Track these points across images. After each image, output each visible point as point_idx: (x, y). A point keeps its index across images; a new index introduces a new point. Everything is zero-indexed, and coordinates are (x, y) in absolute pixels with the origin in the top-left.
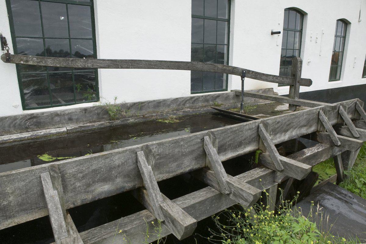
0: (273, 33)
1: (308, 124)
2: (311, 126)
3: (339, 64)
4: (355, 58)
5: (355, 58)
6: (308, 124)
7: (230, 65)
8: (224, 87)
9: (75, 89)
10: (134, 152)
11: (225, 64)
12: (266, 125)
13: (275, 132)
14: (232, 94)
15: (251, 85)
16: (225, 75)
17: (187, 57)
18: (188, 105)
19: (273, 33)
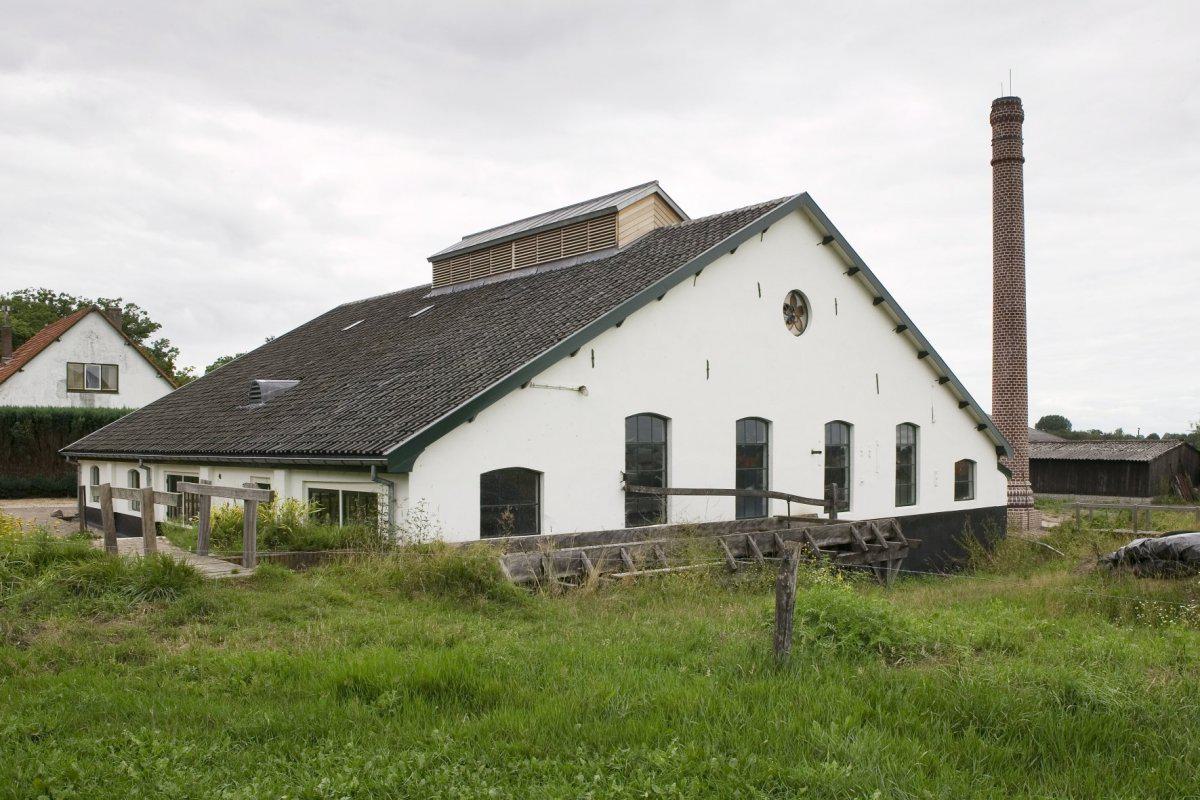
0: (813, 452)
1: (841, 535)
2: (845, 538)
3: (970, 479)
4: (936, 473)
5: (936, 473)
6: (841, 535)
7: (669, 486)
8: (764, 514)
9: (238, 575)
10: (747, 536)
11: (663, 486)
12: (809, 530)
13: (816, 537)
14: (775, 519)
15: (797, 509)
16: (764, 499)
17: (732, 485)
18: (738, 528)
19: (813, 452)
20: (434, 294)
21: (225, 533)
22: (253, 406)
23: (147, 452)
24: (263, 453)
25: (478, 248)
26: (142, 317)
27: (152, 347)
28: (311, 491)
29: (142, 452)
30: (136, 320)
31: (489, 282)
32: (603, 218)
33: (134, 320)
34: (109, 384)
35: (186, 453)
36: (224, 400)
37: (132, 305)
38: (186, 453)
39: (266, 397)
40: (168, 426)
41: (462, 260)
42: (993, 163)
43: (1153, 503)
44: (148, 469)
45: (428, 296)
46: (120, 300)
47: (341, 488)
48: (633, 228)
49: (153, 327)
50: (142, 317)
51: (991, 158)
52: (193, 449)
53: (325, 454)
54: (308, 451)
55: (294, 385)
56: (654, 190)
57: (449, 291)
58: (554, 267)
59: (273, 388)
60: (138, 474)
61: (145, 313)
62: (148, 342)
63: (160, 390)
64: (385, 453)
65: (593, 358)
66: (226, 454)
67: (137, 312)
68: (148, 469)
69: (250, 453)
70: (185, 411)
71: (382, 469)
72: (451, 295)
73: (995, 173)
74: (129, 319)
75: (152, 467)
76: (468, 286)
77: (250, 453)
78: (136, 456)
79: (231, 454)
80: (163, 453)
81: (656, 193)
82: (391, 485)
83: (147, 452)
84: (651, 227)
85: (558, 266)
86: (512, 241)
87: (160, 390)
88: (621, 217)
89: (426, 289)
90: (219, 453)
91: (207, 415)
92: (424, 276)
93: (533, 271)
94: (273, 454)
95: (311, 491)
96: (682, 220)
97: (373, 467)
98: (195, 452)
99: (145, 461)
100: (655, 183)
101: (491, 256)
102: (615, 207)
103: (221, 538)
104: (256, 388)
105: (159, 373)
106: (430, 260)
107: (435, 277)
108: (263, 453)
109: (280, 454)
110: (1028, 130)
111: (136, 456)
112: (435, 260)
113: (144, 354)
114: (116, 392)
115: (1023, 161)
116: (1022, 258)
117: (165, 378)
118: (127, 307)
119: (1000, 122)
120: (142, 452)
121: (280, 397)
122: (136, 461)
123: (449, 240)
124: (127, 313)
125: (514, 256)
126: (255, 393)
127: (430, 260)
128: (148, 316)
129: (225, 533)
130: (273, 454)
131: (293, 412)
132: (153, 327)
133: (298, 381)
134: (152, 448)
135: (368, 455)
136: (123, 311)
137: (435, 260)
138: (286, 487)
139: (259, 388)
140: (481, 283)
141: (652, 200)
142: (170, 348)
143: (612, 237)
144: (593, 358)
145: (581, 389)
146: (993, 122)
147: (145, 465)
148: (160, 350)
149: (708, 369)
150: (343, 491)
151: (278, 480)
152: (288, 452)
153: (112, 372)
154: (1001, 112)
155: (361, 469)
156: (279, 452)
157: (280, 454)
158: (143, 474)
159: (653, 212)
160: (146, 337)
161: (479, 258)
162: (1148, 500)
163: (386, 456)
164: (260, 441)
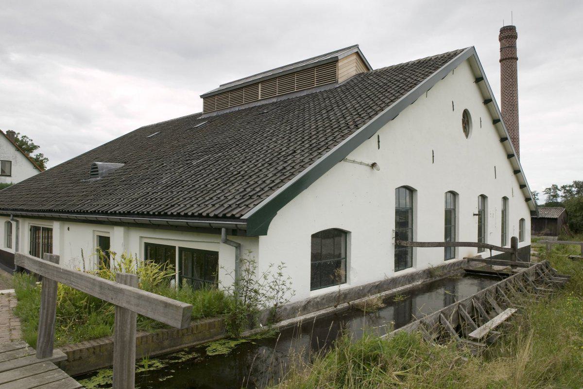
11: (410, 240)
20: (203, 117)
21: (77, 307)
22: (94, 179)
23: (16, 210)
24: (106, 213)
25: (235, 88)
26: (30, 142)
27: (35, 157)
28: (147, 245)
29: (13, 210)
30: (27, 144)
31: (243, 108)
32: (329, 64)
33: (26, 143)
34: (6, 172)
35: (44, 211)
36: (72, 176)
37: (25, 136)
38: (44, 211)
39: (102, 174)
40: (33, 193)
41: (223, 96)
42: (501, 61)
43: (559, 239)
44: (17, 222)
45: (200, 118)
46: (19, 134)
47: (177, 245)
48: (347, 71)
49: (35, 147)
50: (30, 142)
51: (499, 58)
52: (49, 208)
53: (166, 215)
54: (148, 212)
55: (118, 167)
56: (356, 50)
57: (215, 114)
58: (290, 97)
59: (107, 168)
60: (11, 224)
61: (32, 140)
62: (33, 155)
63: (33, 172)
64: (245, 217)
65: (379, 142)
66: (74, 212)
67: (28, 140)
68: (17, 222)
69: (94, 213)
70: (46, 183)
71: (234, 232)
72: (217, 116)
73: (502, 66)
74: (23, 143)
75: (20, 220)
76: (228, 111)
77: (94, 213)
78: (9, 212)
79: (78, 213)
80: (27, 211)
81: (357, 53)
82: (238, 247)
83: (16, 210)
84: (354, 73)
85: (294, 96)
86: (259, 83)
87: (33, 172)
88: (340, 64)
89: (200, 114)
90: (68, 212)
91: (60, 185)
92: (196, 107)
93: (275, 100)
94: (114, 214)
95: (147, 245)
96: (369, 70)
97: (223, 230)
98: (50, 211)
99: (14, 216)
100: (357, 46)
101: (243, 93)
102: (337, 57)
103: (70, 314)
104: (95, 167)
105: (35, 166)
106: (201, 96)
107: (205, 106)
108: (106, 213)
109: (120, 214)
110: (520, 43)
111: (9, 212)
112: (206, 97)
113: (30, 160)
114: (10, 176)
115: (517, 59)
116: (517, 111)
117: (38, 169)
118: (23, 137)
119: (509, 38)
120: (13, 210)
121: (111, 173)
122: (8, 215)
123: (213, 86)
124: (22, 140)
125: (260, 93)
126: (95, 170)
127: (201, 96)
128: (33, 142)
129: (77, 307)
130: (114, 214)
131: (125, 183)
132: (35, 147)
133: (123, 164)
134: (20, 207)
135: (216, 217)
136: (20, 139)
137: (206, 97)
138: (125, 238)
139: (97, 168)
140: (237, 109)
141: (355, 57)
142: (44, 158)
143: (334, 76)
144: (379, 142)
145: (373, 165)
146: (500, 40)
147: (15, 218)
148: (39, 158)
149: (433, 156)
150: (180, 248)
151: (117, 236)
152: (129, 212)
153: (8, 165)
154: (506, 34)
155: (214, 231)
156: (138, 213)
157: (120, 214)
158: (14, 224)
159: (355, 64)
160: (32, 152)
161: (235, 94)
162: (557, 238)
163: (244, 220)
164: (102, 204)
